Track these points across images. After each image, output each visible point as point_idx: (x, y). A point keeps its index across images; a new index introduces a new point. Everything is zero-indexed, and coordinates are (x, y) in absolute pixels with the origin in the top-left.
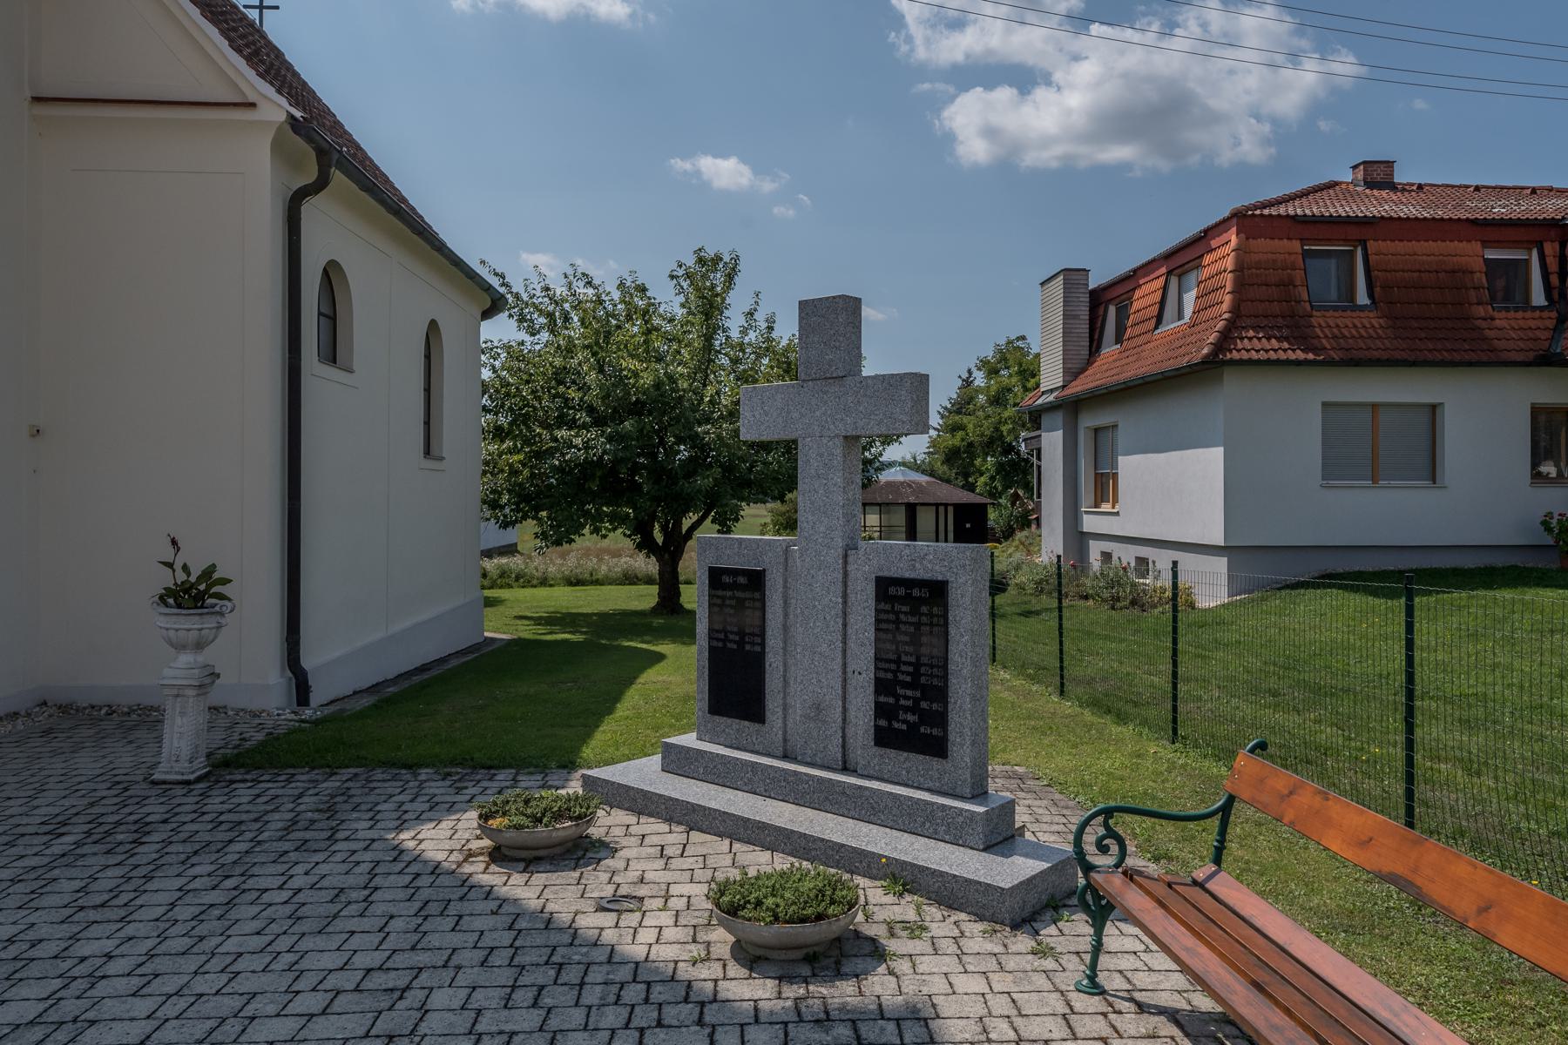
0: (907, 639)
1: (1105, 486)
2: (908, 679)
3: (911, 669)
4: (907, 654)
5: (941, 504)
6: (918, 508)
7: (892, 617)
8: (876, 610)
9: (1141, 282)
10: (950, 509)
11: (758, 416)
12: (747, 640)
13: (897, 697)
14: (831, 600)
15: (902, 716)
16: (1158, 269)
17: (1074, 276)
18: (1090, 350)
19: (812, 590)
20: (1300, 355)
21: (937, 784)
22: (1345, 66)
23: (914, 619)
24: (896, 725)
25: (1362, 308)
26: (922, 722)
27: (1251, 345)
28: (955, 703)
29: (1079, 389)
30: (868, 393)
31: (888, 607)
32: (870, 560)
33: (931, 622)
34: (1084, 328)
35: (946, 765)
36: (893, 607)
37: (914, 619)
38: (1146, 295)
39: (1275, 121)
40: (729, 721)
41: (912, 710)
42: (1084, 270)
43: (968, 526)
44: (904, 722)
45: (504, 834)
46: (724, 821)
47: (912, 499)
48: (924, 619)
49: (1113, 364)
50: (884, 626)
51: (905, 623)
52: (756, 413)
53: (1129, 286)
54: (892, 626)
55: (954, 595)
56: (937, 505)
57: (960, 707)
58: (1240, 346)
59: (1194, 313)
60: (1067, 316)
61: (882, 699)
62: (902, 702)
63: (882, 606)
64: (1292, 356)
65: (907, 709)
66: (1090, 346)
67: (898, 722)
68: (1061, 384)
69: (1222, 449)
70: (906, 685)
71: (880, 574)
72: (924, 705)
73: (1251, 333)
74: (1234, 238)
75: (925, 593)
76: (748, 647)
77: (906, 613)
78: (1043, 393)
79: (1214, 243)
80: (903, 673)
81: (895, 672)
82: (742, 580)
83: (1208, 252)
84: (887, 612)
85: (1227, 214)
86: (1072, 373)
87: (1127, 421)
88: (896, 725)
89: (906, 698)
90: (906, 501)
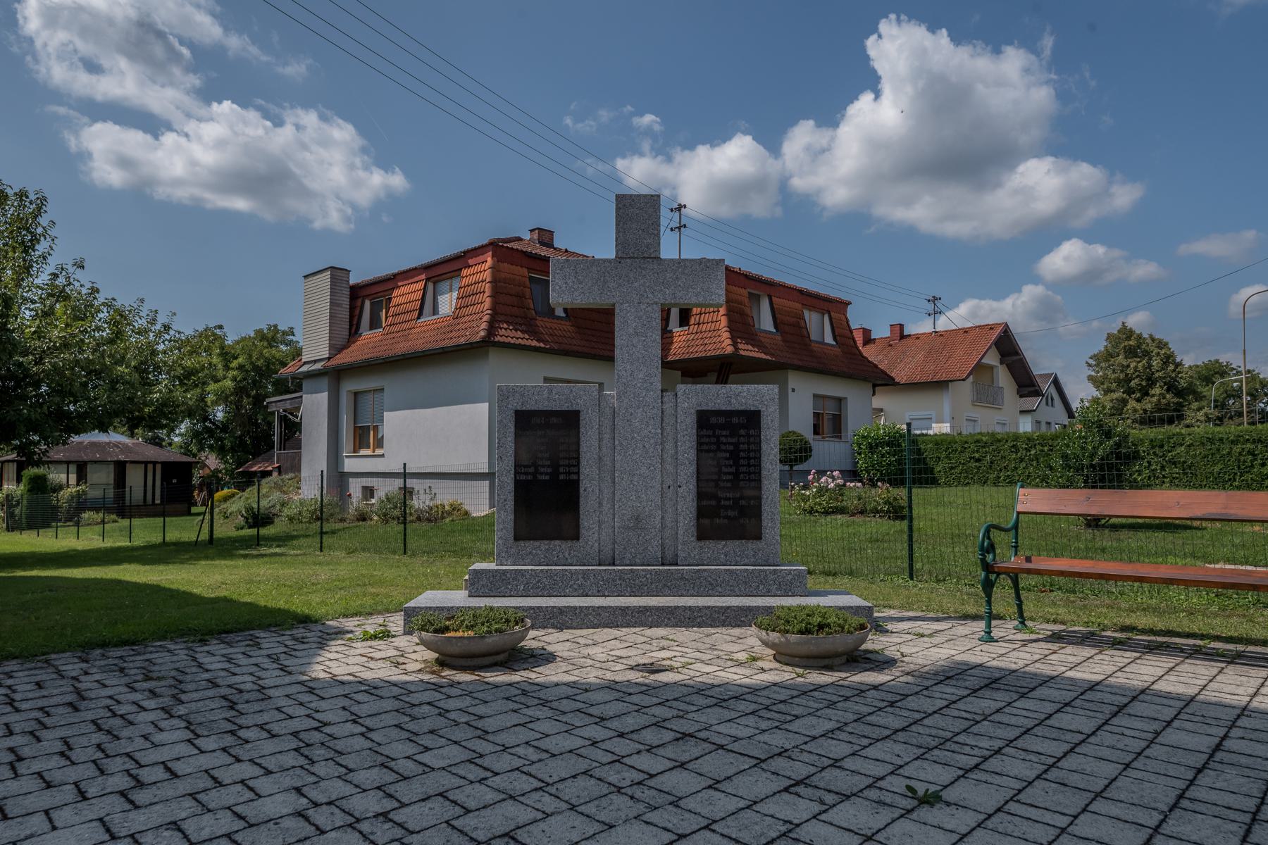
1: (366, 436)
5: (150, 462)
6: (127, 465)
7: (713, 440)
8: (697, 435)
9: (400, 284)
10: (159, 467)
12: (561, 470)
14: (650, 432)
16: (420, 274)
17: (339, 273)
18: (350, 332)
19: (630, 425)
20: (534, 343)
21: (752, 560)
22: (397, 181)
23: (734, 440)
25: (559, 318)
27: (506, 334)
28: (767, 498)
29: (341, 361)
32: (689, 398)
34: (345, 314)
35: (761, 544)
36: (714, 432)
37: (734, 440)
38: (406, 294)
39: (354, 206)
40: (537, 543)
42: (346, 270)
43: (174, 481)
45: (487, 640)
46: (600, 615)
47: (122, 458)
49: (370, 342)
50: (705, 447)
53: (390, 285)
54: (713, 447)
55: (765, 421)
56: (146, 463)
57: (772, 501)
58: (501, 334)
59: (456, 309)
60: (333, 304)
62: (723, 503)
64: (529, 343)
66: (350, 329)
68: (327, 356)
69: (487, 404)
73: (505, 326)
74: (489, 259)
75: (743, 420)
76: (562, 477)
77: (726, 436)
78: (305, 363)
79: (471, 262)
82: (554, 420)
83: (465, 268)
85: (486, 242)
86: (336, 349)
87: (392, 385)
89: (727, 499)
90: (116, 459)
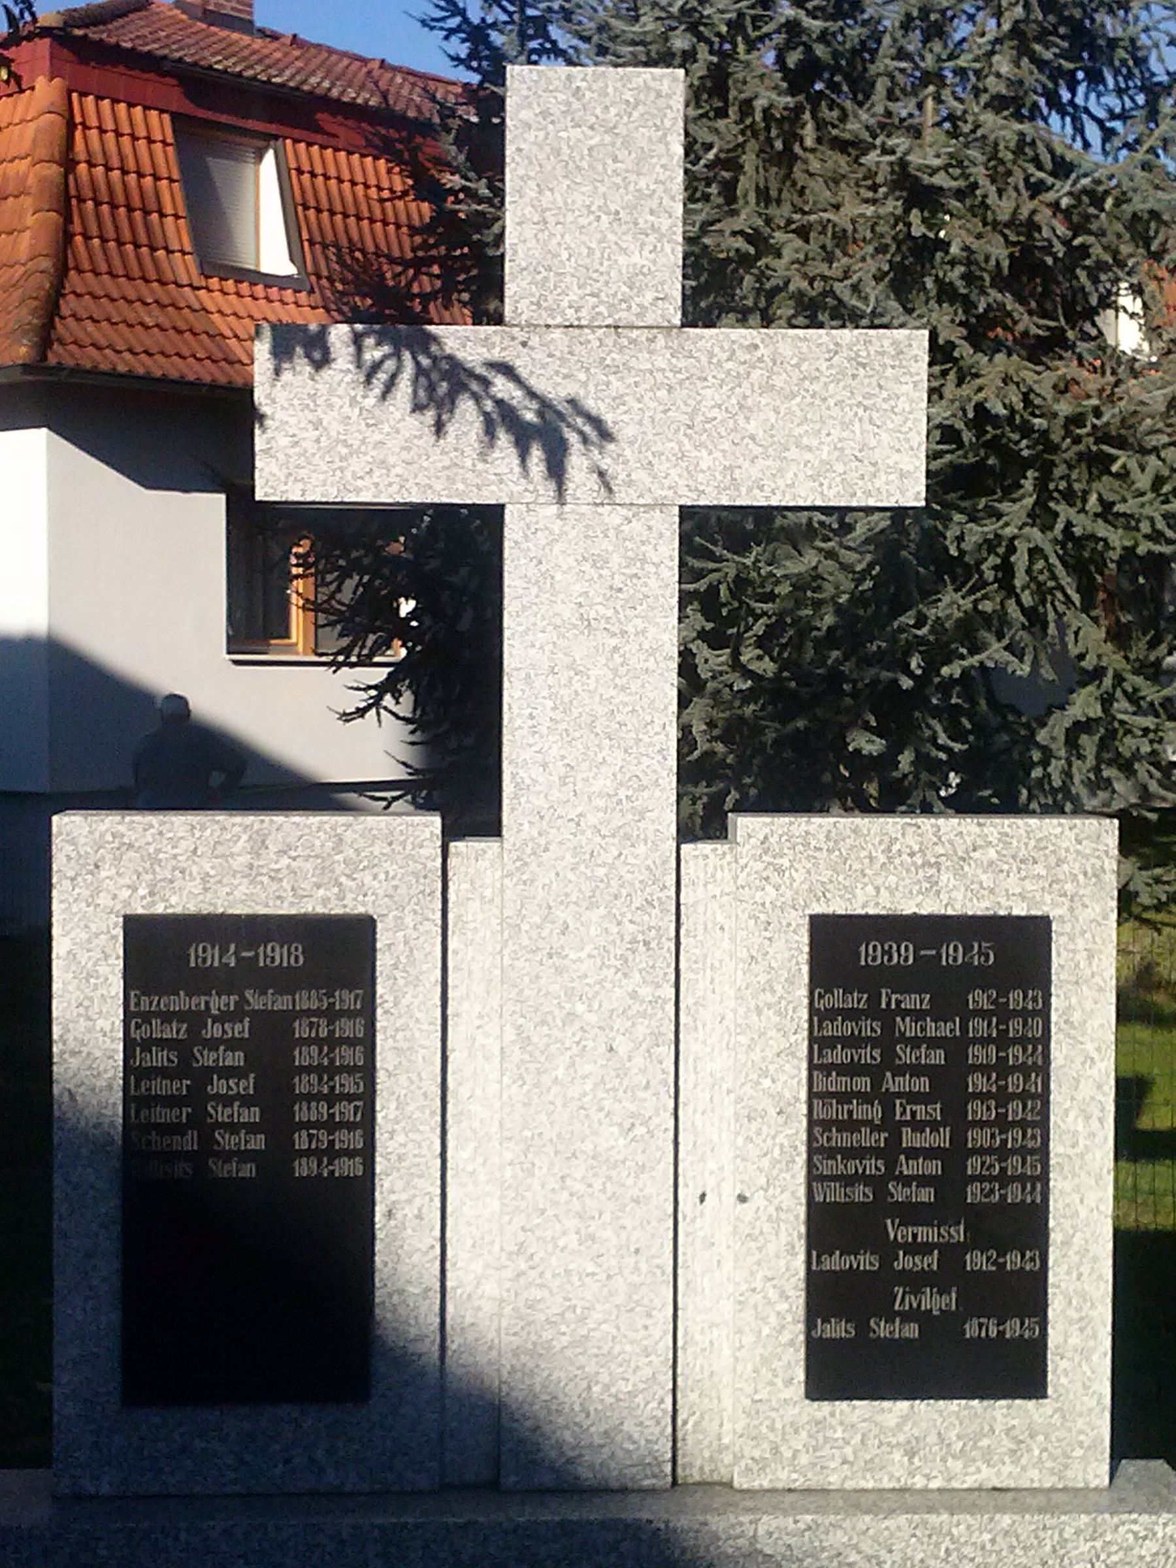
0: (922, 1084)
2: (926, 1195)
3: (934, 1167)
4: (918, 1126)
7: (870, 1028)
8: (812, 1039)
11: (335, 428)
13: (887, 1251)
14: (634, 995)
15: (903, 1300)
19: (559, 971)
23: (944, 1030)
24: (882, 1329)
26: (973, 1305)
30: (778, 381)
31: (857, 1000)
33: (1002, 1061)
36: (874, 999)
37: (944, 1030)
41: (937, 1281)
44: (916, 1070)
48: (979, 1026)
51: (915, 1042)
52: (330, 419)
61: (684, 587)
62: (903, 1262)
63: (836, 999)
65: (916, 1281)
67: (890, 1320)
70: (911, 1214)
71: (818, 909)
72: (977, 1261)
75: (983, 955)
80: (906, 1181)
81: (878, 1184)
82: (278, 955)
84: (850, 1015)
88: (882, 1329)
89: (916, 1248)
